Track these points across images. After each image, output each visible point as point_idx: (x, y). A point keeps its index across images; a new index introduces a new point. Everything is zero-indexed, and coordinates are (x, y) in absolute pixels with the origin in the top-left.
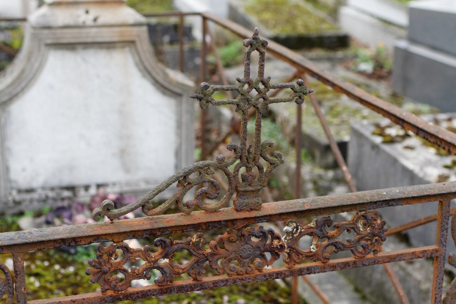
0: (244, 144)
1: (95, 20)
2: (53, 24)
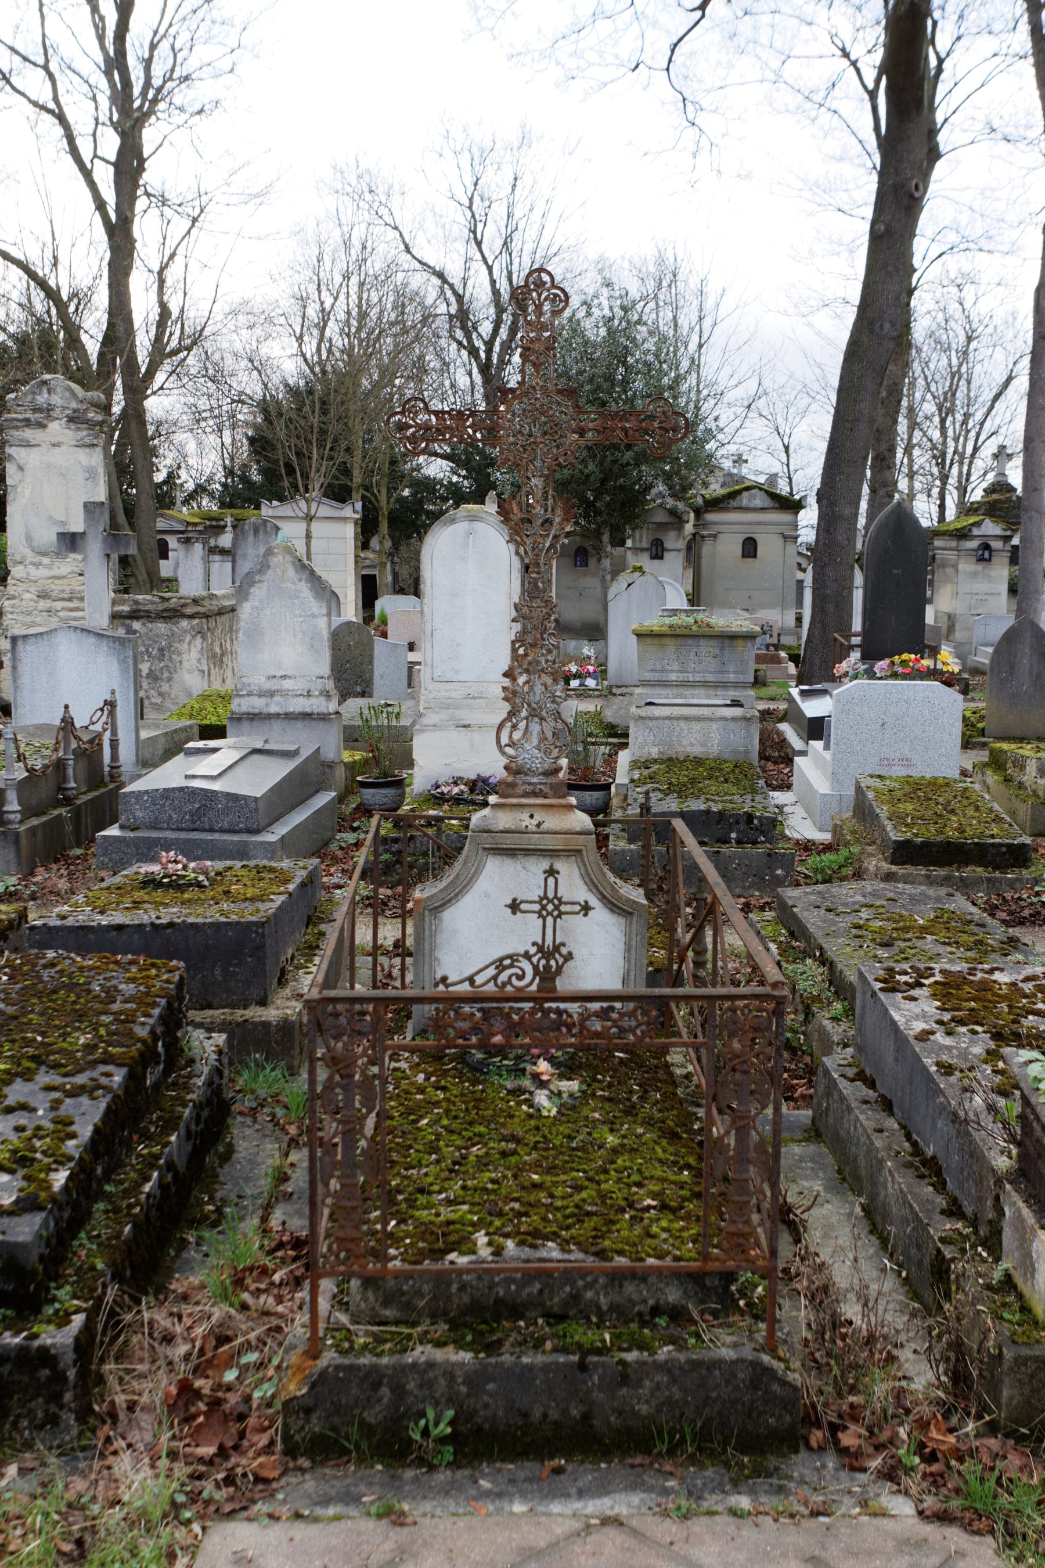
0: (777, 1109)
1: (538, 825)
2: (493, 827)
